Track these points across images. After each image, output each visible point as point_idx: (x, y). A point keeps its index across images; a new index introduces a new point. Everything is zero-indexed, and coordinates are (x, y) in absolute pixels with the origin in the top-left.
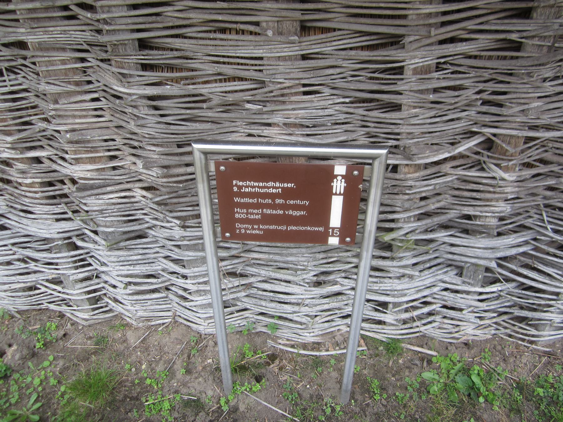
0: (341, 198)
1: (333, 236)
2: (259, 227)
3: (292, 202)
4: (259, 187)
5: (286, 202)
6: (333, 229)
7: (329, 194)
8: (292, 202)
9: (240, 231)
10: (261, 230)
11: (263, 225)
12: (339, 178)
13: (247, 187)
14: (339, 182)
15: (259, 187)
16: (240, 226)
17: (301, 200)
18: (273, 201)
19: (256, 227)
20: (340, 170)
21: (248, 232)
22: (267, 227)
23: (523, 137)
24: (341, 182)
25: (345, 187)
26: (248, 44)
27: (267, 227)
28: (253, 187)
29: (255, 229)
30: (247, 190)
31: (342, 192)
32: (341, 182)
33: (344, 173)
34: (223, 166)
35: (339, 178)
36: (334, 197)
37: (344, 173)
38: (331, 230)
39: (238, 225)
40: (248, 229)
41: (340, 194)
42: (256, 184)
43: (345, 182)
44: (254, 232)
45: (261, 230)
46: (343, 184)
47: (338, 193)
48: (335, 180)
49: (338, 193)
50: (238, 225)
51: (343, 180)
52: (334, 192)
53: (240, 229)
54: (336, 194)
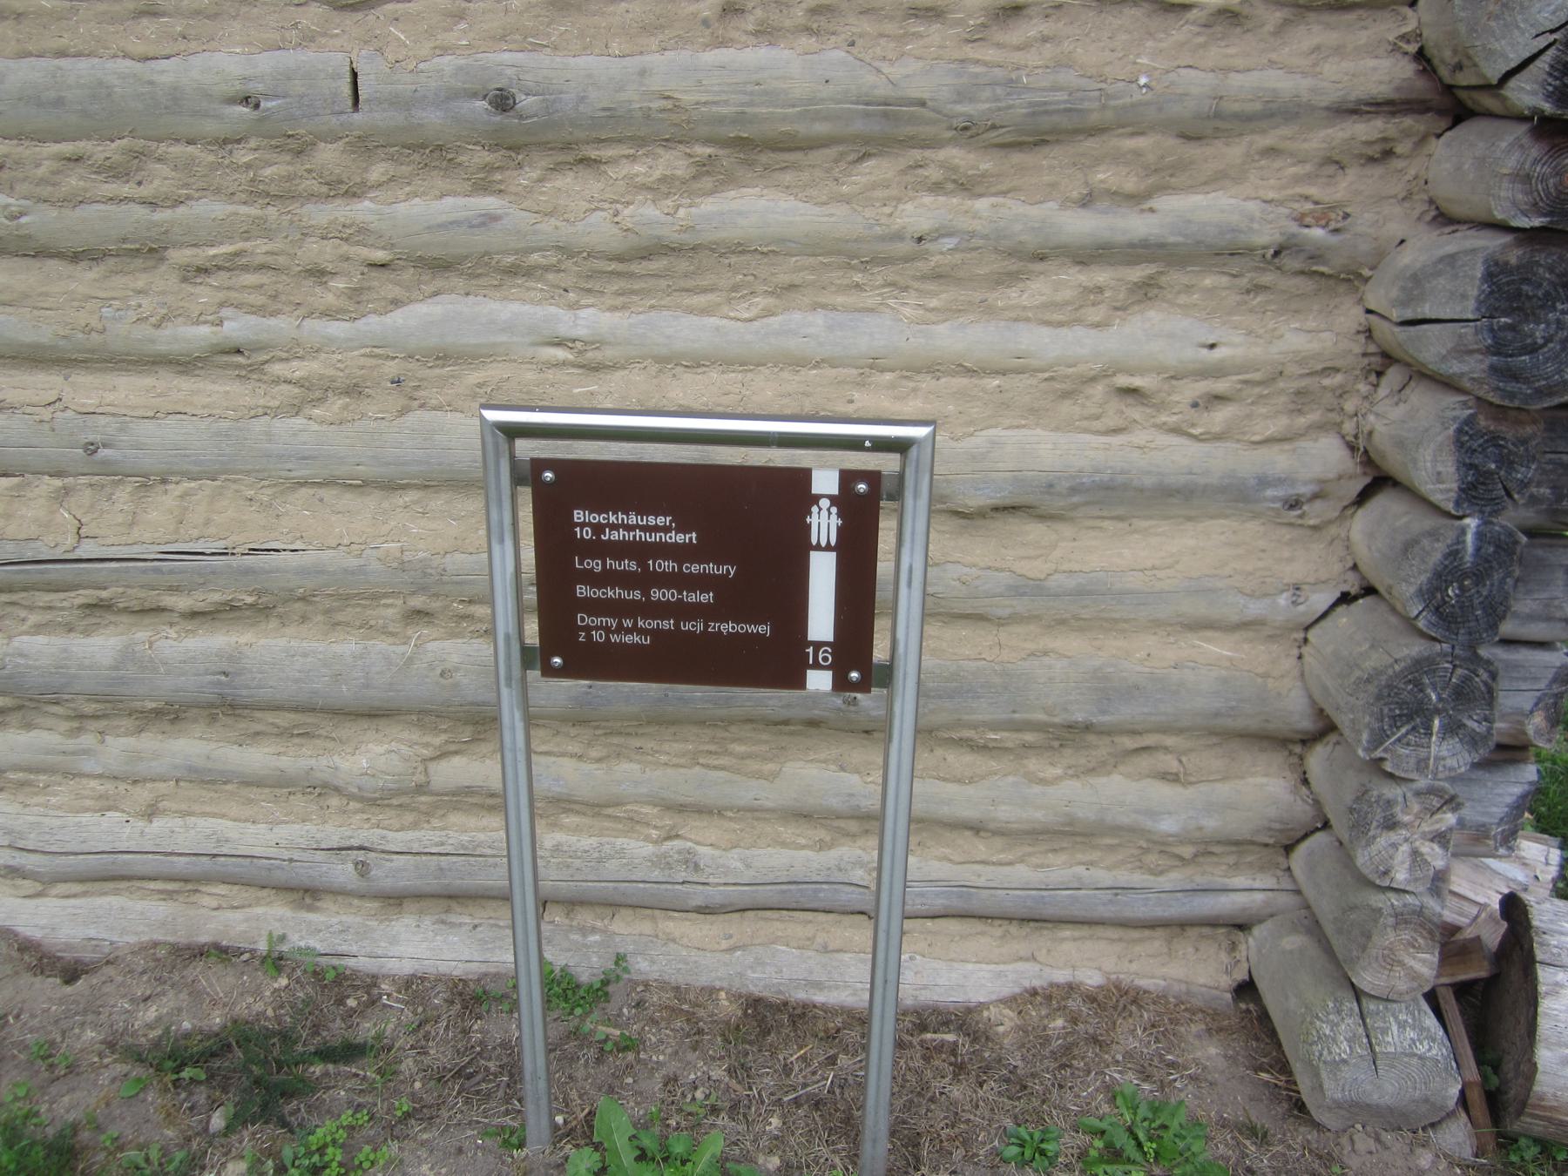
0: (831, 557)
1: (817, 666)
2: (635, 623)
3: (695, 568)
4: (645, 529)
5: (680, 568)
6: (818, 645)
7: (799, 547)
8: (695, 568)
9: (589, 637)
10: (642, 632)
11: (645, 617)
12: (825, 503)
13: (614, 527)
14: (824, 513)
15: (645, 529)
16: (588, 621)
17: (718, 563)
18: (642, 564)
19: (628, 623)
20: (825, 482)
21: (614, 638)
22: (654, 624)
23: (165, 943)
24: (830, 513)
25: (839, 529)
26: (651, 283)
27: (654, 624)
28: (629, 528)
29: (629, 631)
30: (615, 536)
31: (833, 542)
32: (830, 513)
33: (835, 491)
34: (862, 481)
35: (825, 503)
36: (814, 556)
37: (835, 491)
38: (810, 650)
39: (583, 619)
40: (608, 630)
41: (828, 548)
42: (633, 519)
43: (839, 515)
44: (628, 639)
45: (642, 632)
46: (835, 521)
47: (823, 544)
48: (815, 509)
49: (823, 544)
50: (583, 620)
51: (834, 510)
52: (814, 541)
53: (588, 629)
54: (818, 548)
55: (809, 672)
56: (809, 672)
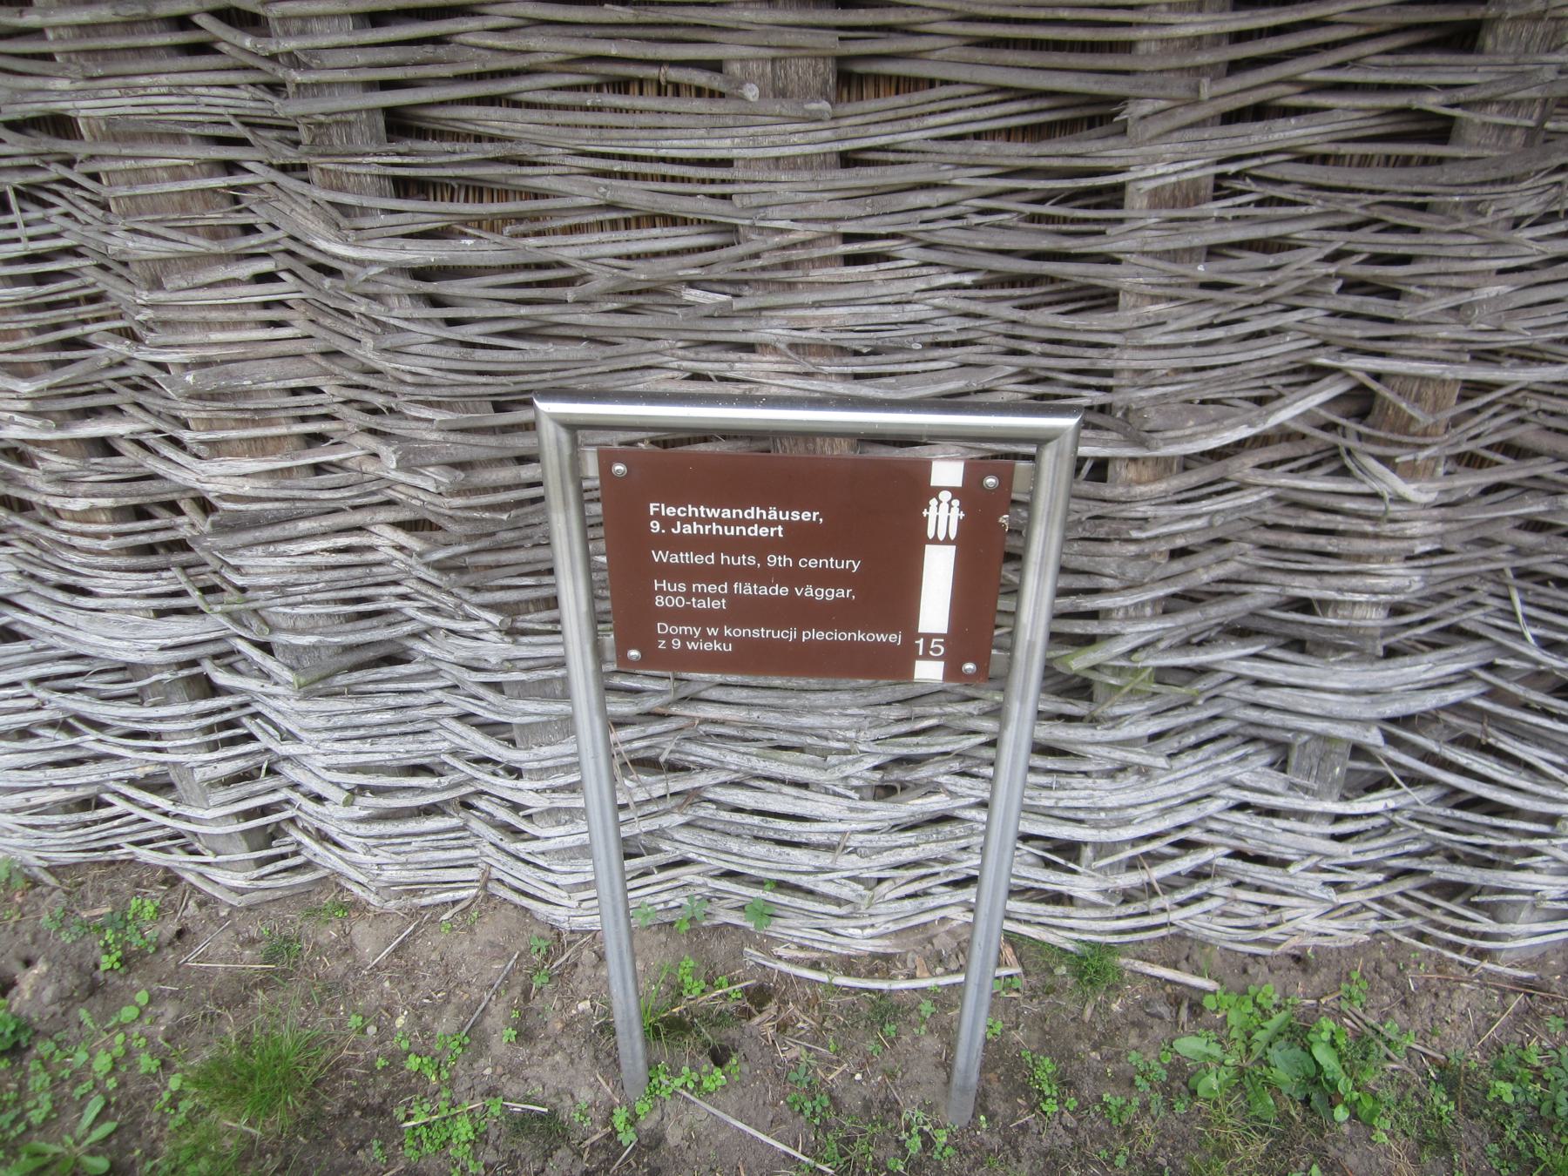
0: (950, 552)
1: (926, 657)
2: (721, 632)
3: (813, 563)
4: (720, 521)
5: (795, 563)
6: (928, 637)
7: (915, 539)
8: (813, 563)
9: (669, 644)
10: (727, 640)
11: (732, 626)
12: (945, 496)
13: (688, 520)
14: (944, 506)
15: (720, 521)
16: (669, 629)
17: (839, 558)
18: (762, 559)
19: (712, 631)
20: (947, 472)
21: (691, 646)
22: (742, 632)
24: (951, 506)
25: (960, 522)
26: (691, 121)
27: (742, 632)
28: (706, 521)
29: (711, 639)
30: (687, 529)
31: (953, 536)
32: (951, 506)
33: (958, 483)
35: (945, 496)
36: (930, 550)
37: (958, 483)
38: (921, 642)
39: (662, 627)
40: (690, 638)
41: (947, 541)
42: (713, 513)
43: (961, 508)
44: (707, 646)
45: (727, 640)
46: (956, 514)
47: (941, 537)
48: (933, 502)
49: (941, 537)
50: (663, 628)
51: (956, 503)
52: (931, 534)
53: (669, 637)
54: (935, 541)
55: (928, 548)
56: (928, 548)
